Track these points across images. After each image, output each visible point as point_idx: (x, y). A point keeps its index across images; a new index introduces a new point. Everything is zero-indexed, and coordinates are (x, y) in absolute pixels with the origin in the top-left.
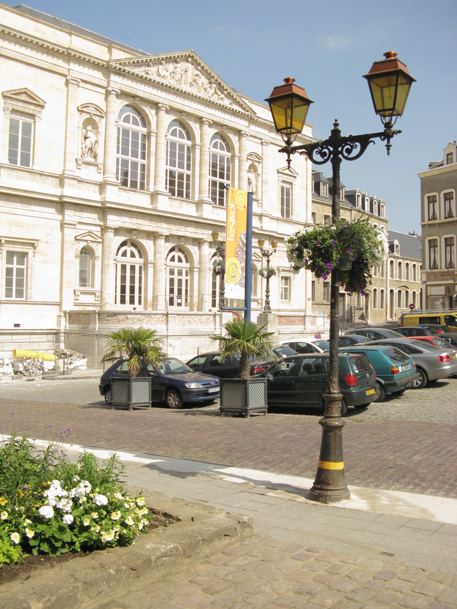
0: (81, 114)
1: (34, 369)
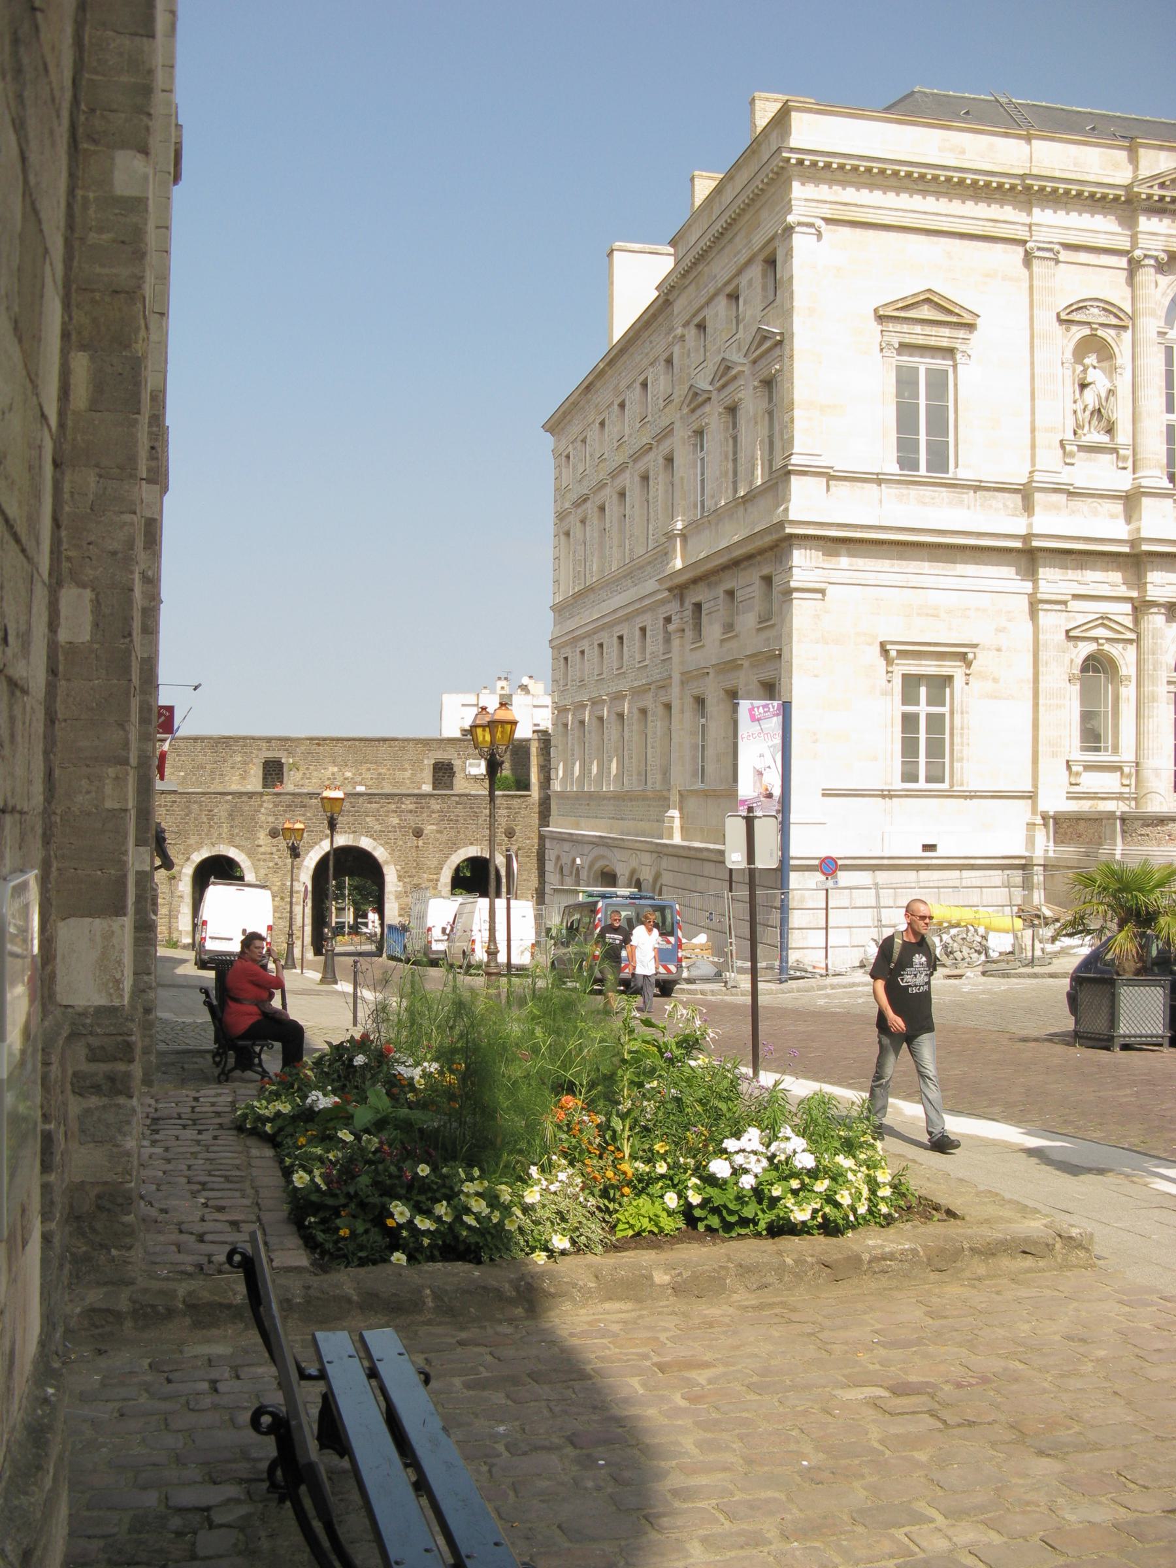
0: (1068, 330)
1: (965, 950)
